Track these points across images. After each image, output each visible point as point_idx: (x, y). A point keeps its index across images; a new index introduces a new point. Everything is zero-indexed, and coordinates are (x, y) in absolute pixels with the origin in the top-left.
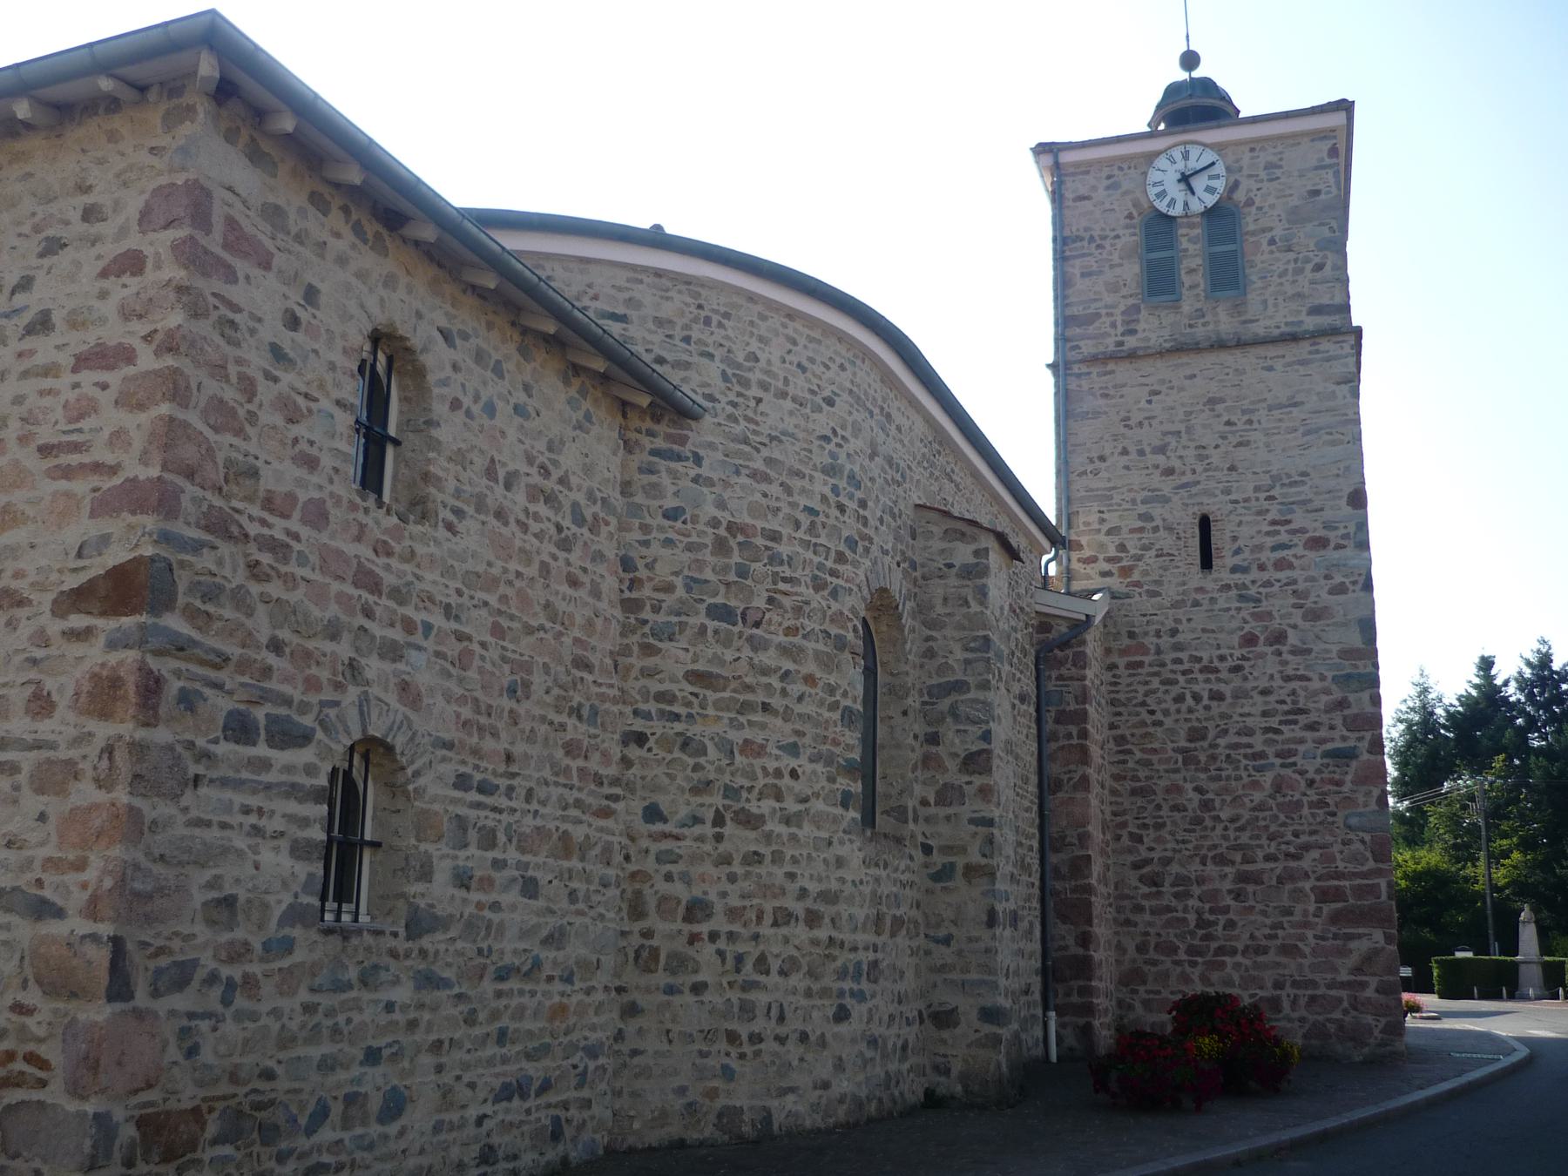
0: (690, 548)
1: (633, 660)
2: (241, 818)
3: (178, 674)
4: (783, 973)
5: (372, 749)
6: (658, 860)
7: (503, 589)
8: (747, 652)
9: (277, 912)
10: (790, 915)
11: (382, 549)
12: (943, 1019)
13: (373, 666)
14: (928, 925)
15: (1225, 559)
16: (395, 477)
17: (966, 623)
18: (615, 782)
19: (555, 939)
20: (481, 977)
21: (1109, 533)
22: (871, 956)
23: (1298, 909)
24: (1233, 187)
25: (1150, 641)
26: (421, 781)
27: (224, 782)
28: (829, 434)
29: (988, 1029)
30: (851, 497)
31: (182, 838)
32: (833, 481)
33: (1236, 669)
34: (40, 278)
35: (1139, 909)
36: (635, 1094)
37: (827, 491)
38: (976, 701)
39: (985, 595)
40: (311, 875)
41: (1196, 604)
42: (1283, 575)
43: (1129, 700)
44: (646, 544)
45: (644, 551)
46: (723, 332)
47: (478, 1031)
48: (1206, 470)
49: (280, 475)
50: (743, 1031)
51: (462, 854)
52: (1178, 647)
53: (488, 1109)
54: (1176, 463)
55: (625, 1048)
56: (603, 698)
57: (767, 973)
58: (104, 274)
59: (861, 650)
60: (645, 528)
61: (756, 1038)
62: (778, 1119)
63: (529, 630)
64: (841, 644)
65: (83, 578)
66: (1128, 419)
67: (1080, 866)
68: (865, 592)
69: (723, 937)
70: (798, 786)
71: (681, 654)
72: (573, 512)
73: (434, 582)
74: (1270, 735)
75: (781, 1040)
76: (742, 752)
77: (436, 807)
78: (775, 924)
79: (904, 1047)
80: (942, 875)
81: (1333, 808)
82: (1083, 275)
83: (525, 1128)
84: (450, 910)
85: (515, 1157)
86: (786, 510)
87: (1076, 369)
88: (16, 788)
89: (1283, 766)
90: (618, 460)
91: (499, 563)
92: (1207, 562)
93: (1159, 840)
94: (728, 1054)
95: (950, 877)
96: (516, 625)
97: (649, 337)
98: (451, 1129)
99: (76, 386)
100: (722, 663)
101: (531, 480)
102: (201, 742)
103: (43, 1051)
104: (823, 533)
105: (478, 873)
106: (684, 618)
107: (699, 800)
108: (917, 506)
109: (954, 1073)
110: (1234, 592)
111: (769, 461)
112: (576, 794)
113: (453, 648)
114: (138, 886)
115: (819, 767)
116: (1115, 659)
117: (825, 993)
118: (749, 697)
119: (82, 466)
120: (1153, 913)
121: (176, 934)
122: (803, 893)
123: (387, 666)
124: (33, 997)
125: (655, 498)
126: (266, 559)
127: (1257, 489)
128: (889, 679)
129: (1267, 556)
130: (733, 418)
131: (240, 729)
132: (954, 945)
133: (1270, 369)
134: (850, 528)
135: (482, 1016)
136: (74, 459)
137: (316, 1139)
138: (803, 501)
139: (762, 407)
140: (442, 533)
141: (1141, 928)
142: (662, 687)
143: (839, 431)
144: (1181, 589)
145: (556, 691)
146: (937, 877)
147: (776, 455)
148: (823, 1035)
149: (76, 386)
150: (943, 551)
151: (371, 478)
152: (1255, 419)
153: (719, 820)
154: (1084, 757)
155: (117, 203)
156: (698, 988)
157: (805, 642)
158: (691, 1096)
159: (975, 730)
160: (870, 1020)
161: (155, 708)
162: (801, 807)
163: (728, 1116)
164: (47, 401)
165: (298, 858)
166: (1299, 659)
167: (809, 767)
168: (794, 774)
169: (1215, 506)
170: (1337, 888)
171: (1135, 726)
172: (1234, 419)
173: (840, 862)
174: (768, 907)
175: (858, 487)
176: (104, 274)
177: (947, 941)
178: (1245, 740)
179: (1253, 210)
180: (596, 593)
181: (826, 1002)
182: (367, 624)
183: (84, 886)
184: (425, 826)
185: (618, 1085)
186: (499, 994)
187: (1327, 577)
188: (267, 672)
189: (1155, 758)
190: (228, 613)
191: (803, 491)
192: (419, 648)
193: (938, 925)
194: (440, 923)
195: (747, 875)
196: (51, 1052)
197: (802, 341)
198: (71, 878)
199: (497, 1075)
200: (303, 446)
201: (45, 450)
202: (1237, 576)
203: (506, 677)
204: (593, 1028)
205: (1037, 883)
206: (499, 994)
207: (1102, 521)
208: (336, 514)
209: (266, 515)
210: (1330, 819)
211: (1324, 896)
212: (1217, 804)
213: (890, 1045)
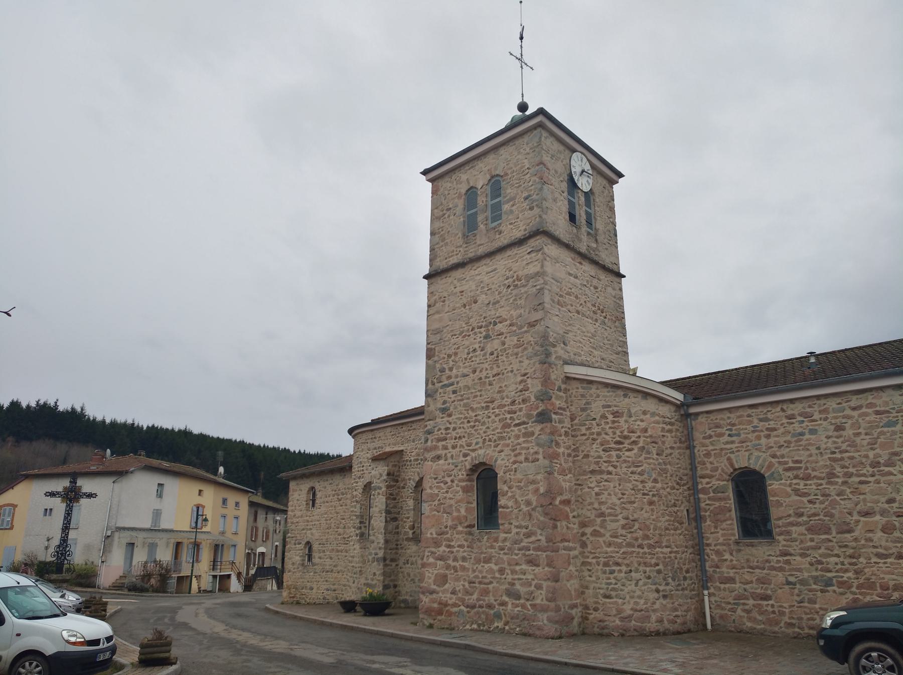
22: (360, 569)
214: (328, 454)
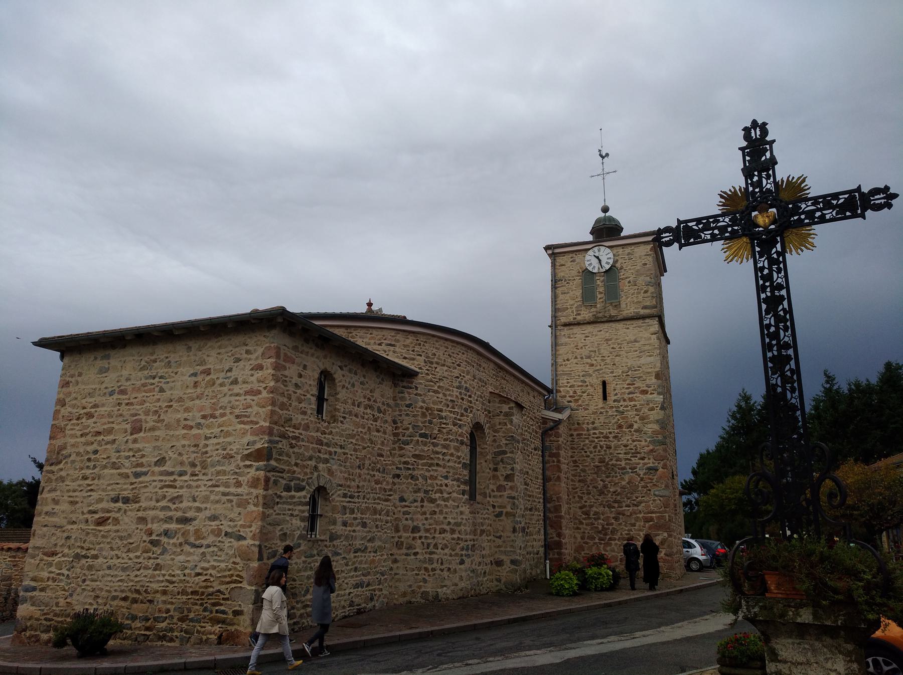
0: (414, 416)
1: (396, 452)
2: (288, 512)
3: (273, 476)
4: (442, 549)
5: (321, 490)
6: (403, 514)
7: (357, 437)
8: (431, 447)
9: (297, 536)
10: (445, 530)
11: (324, 433)
12: (499, 563)
13: (321, 466)
14: (494, 532)
15: (611, 398)
16: (326, 409)
17: (506, 431)
18: (391, 490)
19: (371, 540)
20: (350, 552)
21: (570, 387)
22: (472, 543)
23: (638, 524)
24: (615, 262)
25: (585, 426)
26: (334, 497)
27: (284, 503)
28: (459, 376)
29: (513, 567)
30: (466, 395)
31: (275, 519)
32: (459, 391)
33: (615, 437)
34: (234, 369)
35: (581, 523)
36: (396, 587)
37: (458, 394)
38: (509, 457)
39: (512, 422)
40: (305, 526)
41: (601, 413)
42: (632, 403)
43: (578, 447)
44: (401, 415)
45: (400, 418)
46: (424, 348)
47: (349, 568)
48: (605, 365)
49: (298, 418)
50: (430, 567)
51: (345, 516)
52: (595, 429)
53: (352, 591)
54: (594, 362)
55: (393, 573)
56: (386, 465)
57: (438, 549)
58: (252, 369)
59: (469, 444)
60: (400, 411)
61: (434, 570)
62: (441, 595)
63: (364, 448)
64: (462, 443)
65: (249, 451)
66: (577, 346)
67: (557, 509)
68: (471, 425)
69: (423, 538)
70: (447, 489)
71: (411, 449)
72: (378, 409)
73: (337, 439)
74: (627, 461)
75: (442, 570)
76: (430, 479)
77: (338, 504)
78: (440, 533)
79: (485, 573)
80: (499, 515)
81: (650, 488)
82: (562, 293)
83: (362, 596)
84: (341, 533)
85: (360, 605)
86: (445, 402)
87: (559, 328)
88: (232, 506)
89: (632, 472)
90: (392, 390)
91: (356, 430)
92: (605, 398)
93: (589, 498)
94: (425, 575)
95: (501, 516)
96: (360, 447)
97: (402, 351)
98: (341, 597)
99: (245, 399)
100: (424, 451)
101: (365, 403)
102: (278, 493)
103: (240, 573)
104: (456, 407)
105: (349, 522)
106: (412, 438)
107: (416, 495)
108: (491, 392)
109: (502, 582)
110: (614, 409)
111: (439, 387)
112: (378, 495)
113: (343, 458)
114: (264, 531)
115: (455, 483)
116: (572, 432)
117: (456, 555)
118: (433, 462)
119: (248, 421)
120: (586, 525)
121: (273, 543)
122: (449, 523)
123: (325, 466)
124: (238, 560)
125: (403, 401)
126: (294, 442)
127: (623, 372)
128: (481, 450)
129: (626, 396)
130: (427, 374)
131: (288, 489)
132: (502, 540)
133: (628, 328)
134: (465, 404)
135: (350, 563)
136: (246, 419)
137: (306, 597)
138: (450, 398)
139: (437, 370)
140: (340, 424)
141: (582, 530)
142: (405, 460)
143: (462, 374)
144: (596, 408)
145: (372, 465)
146: (497, 516)
147: (441, 385)
148: (455, 569)
149: (245, 399)
150: (499, 407)
151: (320, 410)
152: (622, 347)
153: (422, 501)
154: (559, 469)
155: (255, 350)
156: (416, 554)
157: (450, 443)
158: (413, 588)
159: (509, 467)
160: (472, 564)
161: (268, 485)
162: (448, 496)
163: (425, 594)
164: (237, 403)
165: (301, 521)
166: (637, 434)
167: (451, 483)
168: (446, 485)
169: (608, 378)
170: (651, 517)
171: (580, 457)
172: (615, 346)
173: (462, 513)
174: (438, 528)
175: (468, 391)
176: (252, 369)
177: (500, 537)
178: (619, 463)
179: (623, 271)
180: (385, 433)
181: (457, 558)
182: (319, 454)
183: (251, 532)
184: (334, 509)
185: (390, 584)
186: (355, 557)
187: (648, 404)
188: (294, 472)
189: (587, 469)
190: (285, 458)
191: (450, 395)
192: (333, 459)
193: (497, 532)
194: (338, 537)
195: (431, 518)
196: (243, 574)
197: (450, 347)
198: (248, 530)
199: (354, 581)
200: (303, 409)
201: (237, 417)
202: (616, 403)
203: (358, 462)
204: (383, 566)
205: (542, 515)
206: (355, 557)
207: (568, 383)
208: (311, 426)
209: (294, 430)
210: (649, 492)
211: (647, 520)
212: (609, 486)
213: (479, 572)
214: (708, 451)
